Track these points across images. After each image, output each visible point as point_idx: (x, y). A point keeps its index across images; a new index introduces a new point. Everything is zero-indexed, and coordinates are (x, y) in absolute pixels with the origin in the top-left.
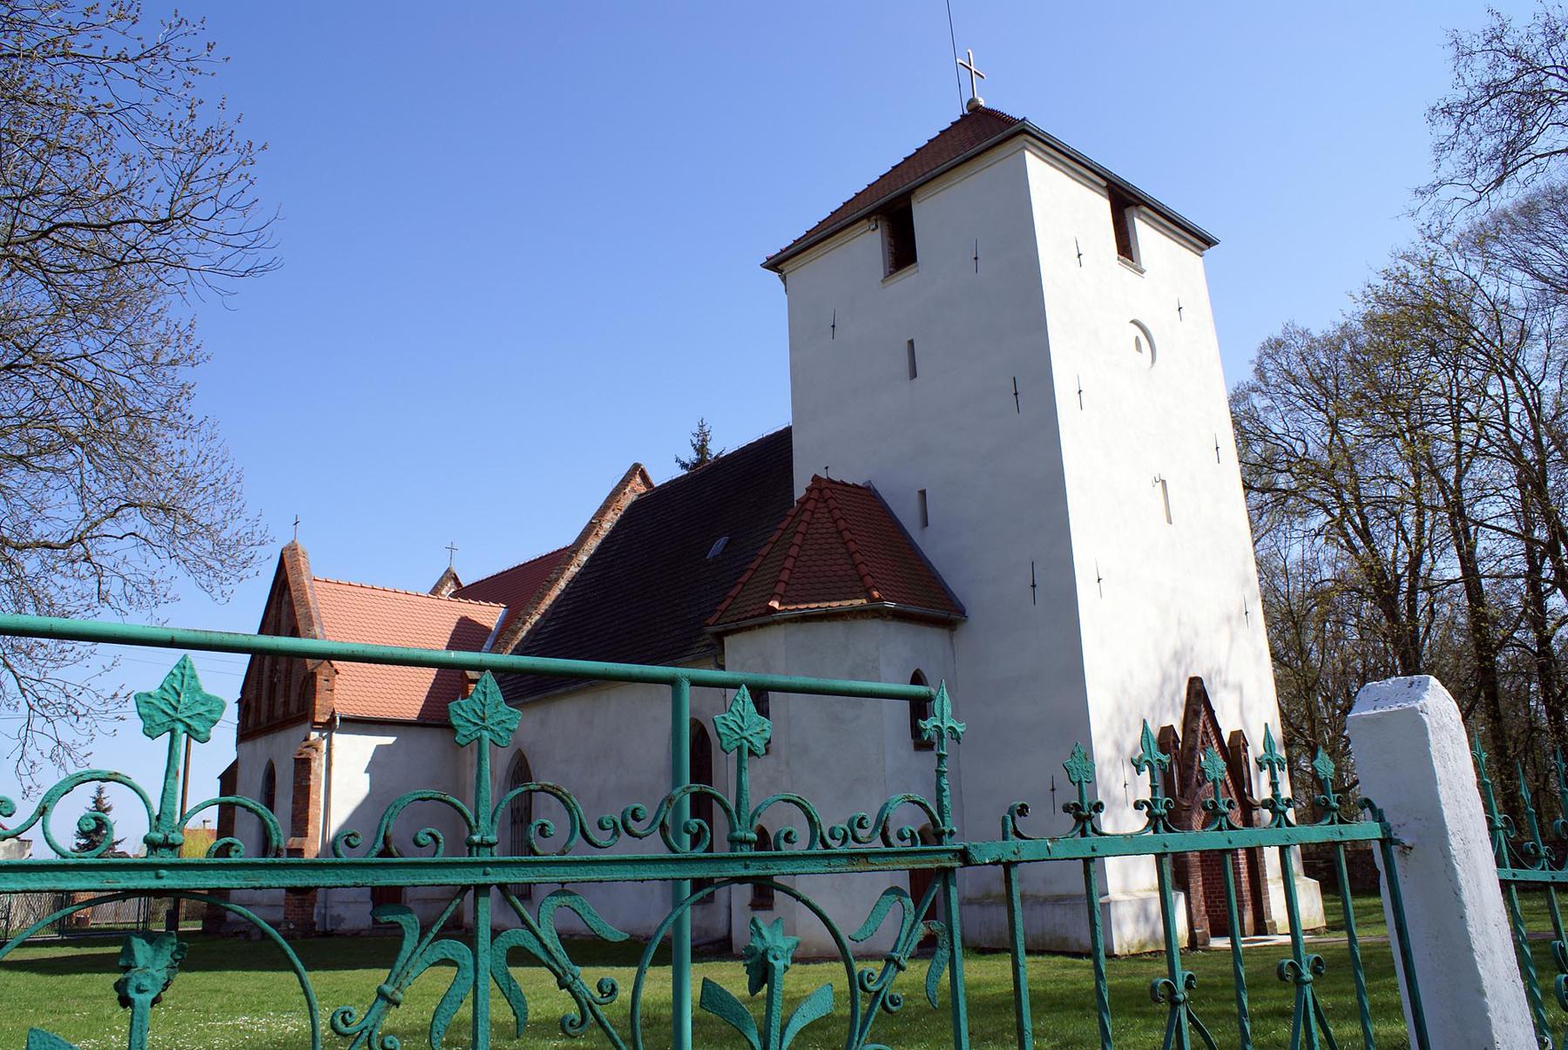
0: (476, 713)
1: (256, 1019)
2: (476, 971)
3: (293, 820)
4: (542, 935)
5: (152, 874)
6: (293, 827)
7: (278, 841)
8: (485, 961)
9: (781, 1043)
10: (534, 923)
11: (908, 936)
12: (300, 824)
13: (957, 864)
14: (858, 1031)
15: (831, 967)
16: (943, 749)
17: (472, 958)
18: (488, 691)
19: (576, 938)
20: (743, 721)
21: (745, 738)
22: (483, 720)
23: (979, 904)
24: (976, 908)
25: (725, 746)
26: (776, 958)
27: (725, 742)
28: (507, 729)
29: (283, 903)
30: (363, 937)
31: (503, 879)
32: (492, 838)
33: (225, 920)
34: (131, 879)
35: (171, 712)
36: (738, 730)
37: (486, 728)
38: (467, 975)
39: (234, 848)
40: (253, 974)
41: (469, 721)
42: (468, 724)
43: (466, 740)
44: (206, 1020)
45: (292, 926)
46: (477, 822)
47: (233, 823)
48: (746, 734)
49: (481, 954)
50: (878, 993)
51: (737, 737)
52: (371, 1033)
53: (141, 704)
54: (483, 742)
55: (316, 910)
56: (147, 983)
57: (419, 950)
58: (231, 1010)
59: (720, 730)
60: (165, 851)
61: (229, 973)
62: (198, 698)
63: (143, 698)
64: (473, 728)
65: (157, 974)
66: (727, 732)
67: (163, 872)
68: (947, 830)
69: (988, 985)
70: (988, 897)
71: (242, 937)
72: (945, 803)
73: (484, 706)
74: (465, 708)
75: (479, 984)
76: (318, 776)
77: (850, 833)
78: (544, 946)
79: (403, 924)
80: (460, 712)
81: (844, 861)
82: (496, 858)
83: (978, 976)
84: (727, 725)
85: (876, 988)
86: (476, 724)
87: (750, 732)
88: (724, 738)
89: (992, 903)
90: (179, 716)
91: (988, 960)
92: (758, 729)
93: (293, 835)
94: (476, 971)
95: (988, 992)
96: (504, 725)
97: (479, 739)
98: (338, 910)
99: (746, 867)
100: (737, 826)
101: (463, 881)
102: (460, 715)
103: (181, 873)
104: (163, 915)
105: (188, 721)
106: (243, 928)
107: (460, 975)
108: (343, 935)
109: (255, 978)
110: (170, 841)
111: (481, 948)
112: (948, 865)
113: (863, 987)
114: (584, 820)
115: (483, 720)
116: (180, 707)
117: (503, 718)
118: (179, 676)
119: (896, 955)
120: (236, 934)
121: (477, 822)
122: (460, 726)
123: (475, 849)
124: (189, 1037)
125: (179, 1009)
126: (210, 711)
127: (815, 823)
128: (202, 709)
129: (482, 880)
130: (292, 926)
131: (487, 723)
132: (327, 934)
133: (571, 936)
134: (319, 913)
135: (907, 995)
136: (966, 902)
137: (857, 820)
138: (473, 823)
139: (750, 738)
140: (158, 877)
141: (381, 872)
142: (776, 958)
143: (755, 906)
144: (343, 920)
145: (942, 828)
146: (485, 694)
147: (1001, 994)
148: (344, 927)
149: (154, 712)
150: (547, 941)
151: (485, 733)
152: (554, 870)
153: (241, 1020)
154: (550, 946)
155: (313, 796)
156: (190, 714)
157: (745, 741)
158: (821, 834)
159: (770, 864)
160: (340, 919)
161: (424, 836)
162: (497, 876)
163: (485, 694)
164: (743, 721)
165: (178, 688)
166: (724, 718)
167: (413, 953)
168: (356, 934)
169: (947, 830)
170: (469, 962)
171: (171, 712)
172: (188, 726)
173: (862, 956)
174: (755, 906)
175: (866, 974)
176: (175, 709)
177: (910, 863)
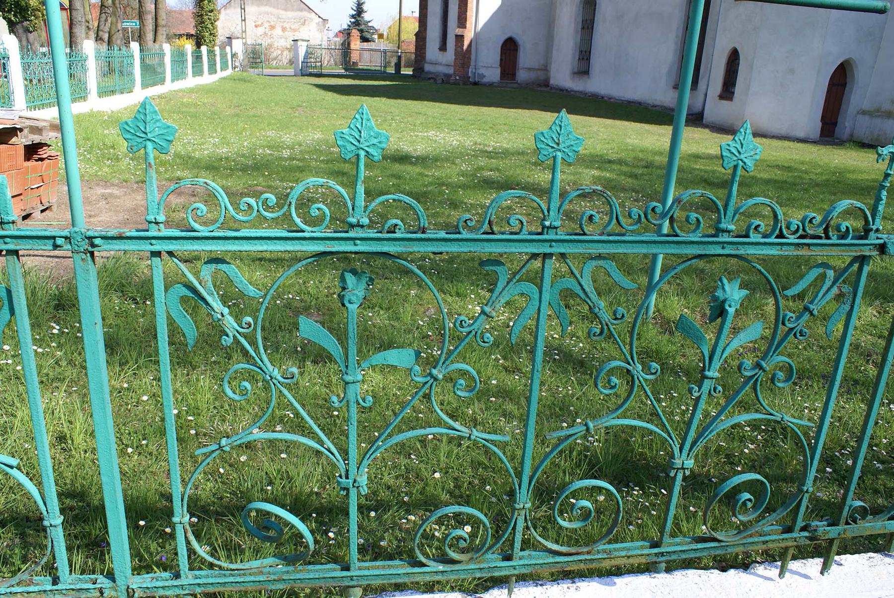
0: (553, 140)
1: (438, 133)
2: (540, 302)
3: (458, 19)
4: (583, 283)
5: (352, 242)
6: (458, 22)
7: (424, 223)
8: (546, 296)
9: (722, 354)
10: (578, 276)
11: (824, 295)
12: (462, 22)
13: (875, 253)
14: (773, 349)
15: (761, 141)
16: (891, 169)
17: (538, 294)
18: (563, 125)
19: (612, 100)
20: (742, 147)
21: (741, 160)
22: (558, 144)
23: (869, 115)
24: (867, 117)
25: (725, 165)
26: (730, 306)
27: (726, 162)
28: (574, 151)
29: (453, 64)
30: (495, 86)
31: (563, 251)
32: (557, 223)
33: (423, 71)
34: (341, 245)
35: (356, 143)
36: (737, 154)
37: (559, 150)
38: (534, 303)
39: (398, 227)
40: (437, 104)
41: (548, 145)
42: (548, 147)
43: (546, 158)
44: (414, 130)
45: (458, 78)
46: (548, 212)
47: (427, 9)
48: (742, 157)
49: (544, 292)
50: (792, 329)
51: (735, 158)
52: (476, 333)
53: (338, 139)
54: (557, 160)
55: (470, 70)
56: (354, 299)
57: (507, 289)
58: (426, 126)
59: (724, 154)
60: (358, 229)
61: (426, 102)
62: (372, 134)
63: (339, 135)
64: (551, 150)
65: (359, 294)
66: (729, 155)
67: (358, 242)
68: (874, 228)
69: (861, 172)
70: (878, 111)
71: (432, 81)
72: (880, 209)
73: (559, 135)
74: (546, 136)
75: (541, 309)
76: (472, 24)
77: (801, 228)
78: (583, 290)
79: (498, 271)
80: (543, 139)
81: (792, 248)
82: (558, 237)
83: (855, 163)
84: (730, 150)
85: (791, 326)
86: (552, 147)
87: (745, 155)
88: (726, 159)
89: (880, 116)
90: (361, 146)
91: (866, 152)
92: (752, 153)
93: (459, 27)
94: (540, 302)
95: (860, 177)
96: (571, 148)
97: (555, 158)
98: (482, 71)
99: (723, 248)
100: (723, 220)
101: (536, 251)
102: (543, 141)
103: (368, 242)
104: (393, 64)
105: (367, 149)
106: (433, 76)
107: (530, 303)
108: (484, 85)
109: (438, 107)
110: (361, 223)
111: (544, 289)
112: (867, 254)
113: (783, 324)
114: (619, 213)
115: (558, 144)
116: (362, 140)
117: (572, 143)
118: (360, 120)
119: (811, 307)
120: (429, 79)
121: (548, 212)
122: (541, 148)
123: (546, 230)
124: (406, 141)
125: (401, 122)
126: (380, 142)
127: (778, 220)
128: (375, 141)
129: (548, 250)
130: (458, 78)
131: (561, 147)
132: (476, 84)
133: (610, 98)
134: (472, 72)
135: (806, 170)
136: (871, 275)
137: (808, 219)
138: (546, 213)
139: (745, 160)
140: (355, 245)
141: (486, 244)
142: (730, 306)
143: (721, 97)
144: (485, 76)
145: (871, 227)
146: (560, 126)
147: (867, 180)
148: (485, 80)
149: (346, 144)
150: (585, 287)
151: (559, 154)
152: (595, 245)
153: (431, 133)
154: (587, 289)
155: (469, 5)
156: (368, 144)
157: (740, 162)
158: (781, 227)
159: (740, 247)
160: (483, 76)
161: (514, 221)
162: (558, 249)
163: (560, 126)
164: (742, 147)
165: (360, 127)
166: (729, 145)
167: (503, 289)
168: (491, 85)
169: (874, 228)
170: (537, 296)
171: (356, 143)
172: (367, 152)
173: (782, 137)
174: (721, 97)
175: (788, 317)
176: (359, 141)
177: (840, 251)
